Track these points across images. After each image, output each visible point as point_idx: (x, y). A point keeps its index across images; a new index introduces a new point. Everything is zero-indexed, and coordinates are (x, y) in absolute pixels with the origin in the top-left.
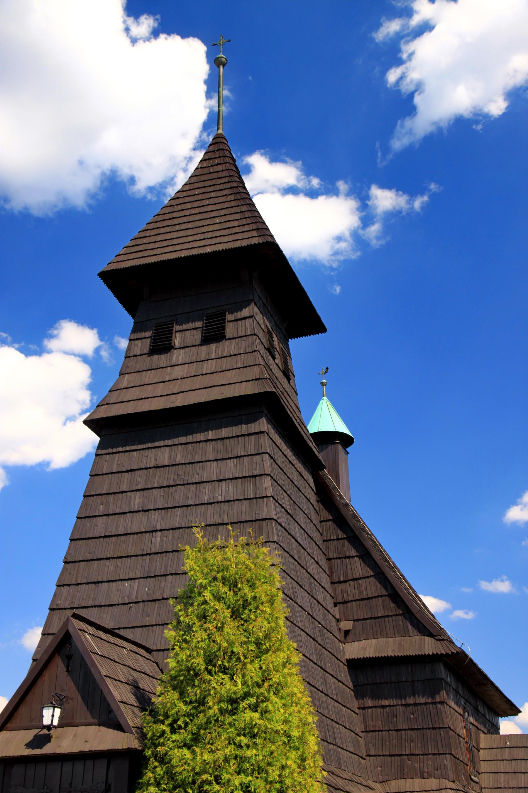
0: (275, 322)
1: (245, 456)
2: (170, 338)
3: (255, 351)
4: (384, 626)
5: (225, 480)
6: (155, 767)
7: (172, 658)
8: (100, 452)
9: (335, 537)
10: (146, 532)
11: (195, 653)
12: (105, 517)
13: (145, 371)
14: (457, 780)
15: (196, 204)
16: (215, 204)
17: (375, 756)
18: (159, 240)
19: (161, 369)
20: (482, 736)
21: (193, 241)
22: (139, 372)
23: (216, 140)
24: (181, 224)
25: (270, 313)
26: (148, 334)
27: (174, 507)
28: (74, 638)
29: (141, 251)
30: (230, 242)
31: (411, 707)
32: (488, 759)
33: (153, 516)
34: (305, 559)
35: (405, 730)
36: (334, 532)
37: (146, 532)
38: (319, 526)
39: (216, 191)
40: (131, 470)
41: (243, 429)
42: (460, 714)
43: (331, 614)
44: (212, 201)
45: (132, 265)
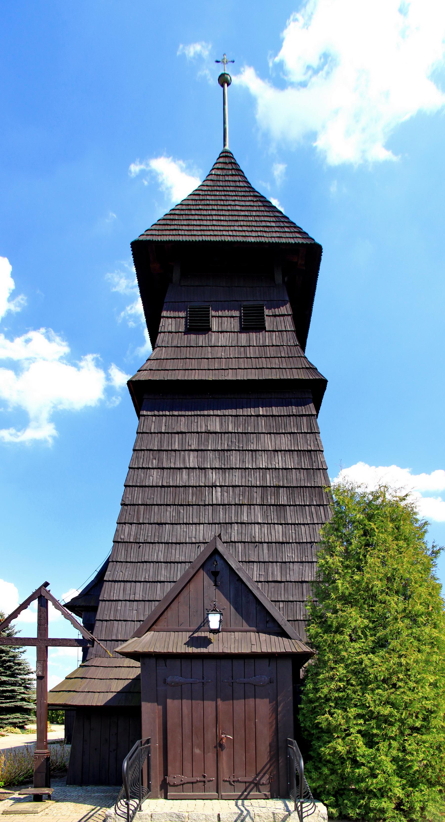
40: (182, 433)
41: (294, 410)
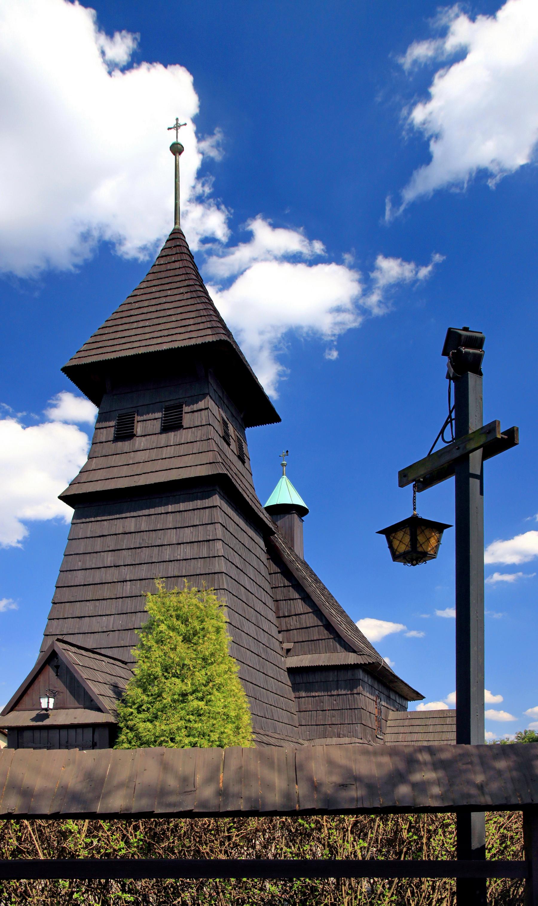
0: (231, 413)
1: (200, 525)
2: (132, 428)
3: (209, 439)
4: (318, 646)
5: (183, 543)
6: (128, 733)
7: (137, 668)
8: (75, 521)
9: (282, 585)
10: (118, 582)
11: (154, 665)
12: (83, 571)
13: (111, 455)
15: (153, 302)
16: (172, 302)
18: (117, 337)
19: (125, 454)
20: (391, 712)
21: (150, 339)
22: (106, 456)
23: (173, 236)
24: (139, 321)
25: (226, 405)
26: (112, 423)
27: (141, 564)
28: (59, 655)
29: (101, 347)
30: (185, 339)
33: (123, 570)
34: (253, 601)
35: (329, 710)
36: (282, 581)
37: (118, 582)
38: (268, 577)
39: (173, 289)
40: (103, 536)
41: (199, 503)
42: (373, 700)
43: (275, 638)
44: (168, 299)
45: (92, 361)
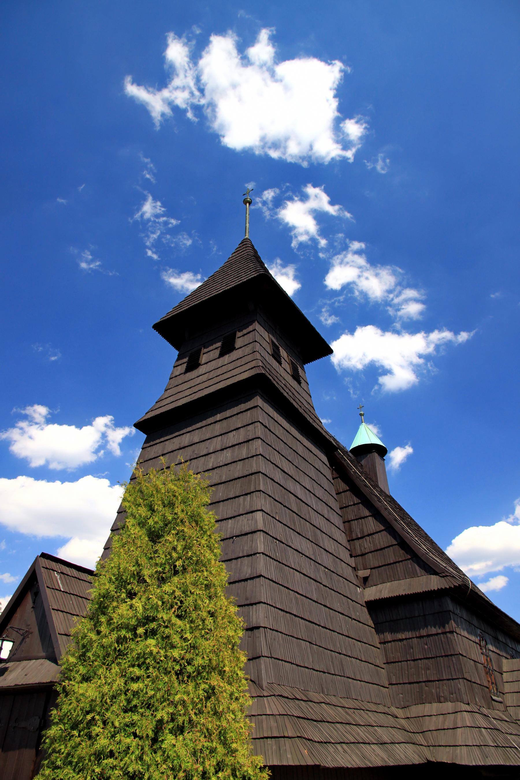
3: (255, 352)
9: (352, 503)
14: (471, 702)
17: (397, 684)
20: (504, 661)
31: (425, 638)
32: (510, 680)
35: (421, 659)
41: (243, 407)
43: (345, 562)
